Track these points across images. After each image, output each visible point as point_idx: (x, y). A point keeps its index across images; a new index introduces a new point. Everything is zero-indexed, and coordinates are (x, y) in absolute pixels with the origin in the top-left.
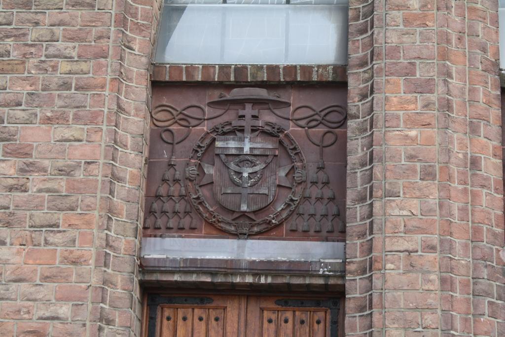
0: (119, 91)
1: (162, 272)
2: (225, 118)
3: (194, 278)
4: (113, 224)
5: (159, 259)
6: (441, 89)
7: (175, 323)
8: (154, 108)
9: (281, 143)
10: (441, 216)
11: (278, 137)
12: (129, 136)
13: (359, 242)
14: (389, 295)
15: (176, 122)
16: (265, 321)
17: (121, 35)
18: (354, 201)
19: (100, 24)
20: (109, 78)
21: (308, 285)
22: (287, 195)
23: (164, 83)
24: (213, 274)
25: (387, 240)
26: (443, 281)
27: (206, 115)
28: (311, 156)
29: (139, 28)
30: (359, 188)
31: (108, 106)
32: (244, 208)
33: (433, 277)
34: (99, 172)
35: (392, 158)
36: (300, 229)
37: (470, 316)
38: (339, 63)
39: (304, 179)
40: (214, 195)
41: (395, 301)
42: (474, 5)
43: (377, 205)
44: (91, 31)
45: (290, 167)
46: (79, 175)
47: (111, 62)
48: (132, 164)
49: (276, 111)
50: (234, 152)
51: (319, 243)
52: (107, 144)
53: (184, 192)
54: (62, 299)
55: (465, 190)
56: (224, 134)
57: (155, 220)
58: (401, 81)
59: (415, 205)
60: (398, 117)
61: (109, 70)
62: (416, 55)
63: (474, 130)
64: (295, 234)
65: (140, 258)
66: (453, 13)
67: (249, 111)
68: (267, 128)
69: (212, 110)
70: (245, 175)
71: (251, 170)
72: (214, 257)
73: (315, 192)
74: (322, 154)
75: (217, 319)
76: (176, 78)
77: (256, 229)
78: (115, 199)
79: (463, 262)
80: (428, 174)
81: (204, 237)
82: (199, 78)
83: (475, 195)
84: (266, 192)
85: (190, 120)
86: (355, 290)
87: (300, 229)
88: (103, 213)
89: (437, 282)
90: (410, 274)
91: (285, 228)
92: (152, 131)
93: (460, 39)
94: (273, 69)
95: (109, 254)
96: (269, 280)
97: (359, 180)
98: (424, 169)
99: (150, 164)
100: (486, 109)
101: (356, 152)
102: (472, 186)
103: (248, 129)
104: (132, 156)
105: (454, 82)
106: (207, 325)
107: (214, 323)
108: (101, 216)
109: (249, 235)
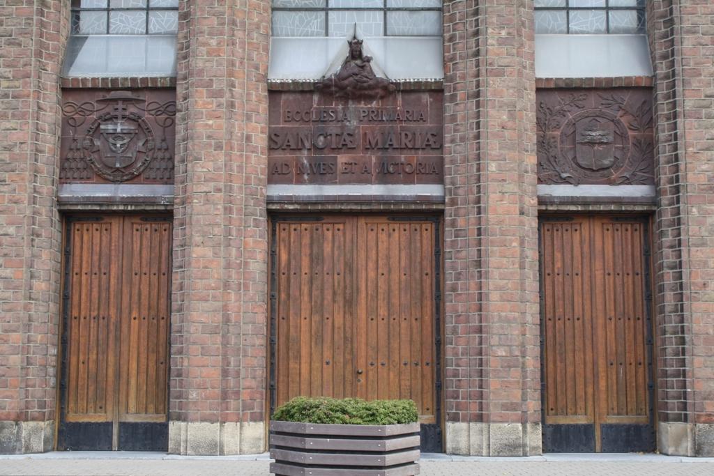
0: (38, 98)
1: (71, 205)
2: (107, 110)
3: (89, 208)
4: (39, 179)
5: (68, 197)
6: (228, 95)
7: (82, 232)
8: (63, 104)
9: (139, 125)
10: (226, 171)
11: (138, 121)
12: (46, 125)
13: (181, 186)
14: (194, 218)
15: (77, 113)
16: (134, 230)
17: (38, 63)
18: (178, 162)
19: (25, 56)
20: (32, 90)
21: (156, 210)
22: (143, 157)
23: (68, 90)
24: (100, 205)
25: (194, 186)
26: (225, 209)
27: (95, 109)
28: (157, 133)
29: (50, 57)
30: (182, 154)
31: (32, 108)
32: (118, 165)
33: (219, 207)
34: (28, 149)
35: (198, 137)
36: (151, 177)
37: (242, 228)
38: (173, 76)
39: (153, 147)
40: (100, 158)
41: (198, 221)
42: (251, 41)
43: (189, 165)
44: (20, 61)
45: (144, 140)
46: (17, 150)
47: (33, 80)
48: (49, 142)
49: (137, 106)
50: (111, 131)
51: (162, 185)
52: (37, 129)
53: (82, 157)
54: (10, 224)
55: (241, 155)
56: (106, 120)
57: (68, 170)
58: (204, 90)
59: (210, 165)
60: (202, 113)
61: (32, 85)
62: (213, 74)
63: (249, 118)
64: (149, 180)
65: (57, 196)
66: (238, 47)
67: (120, 105)
68: (132, 116)
69: (98, 105)
70: (118, 145)
71: (121, 143)
72: (101, 195)
73: (160, 154)
74: (164, 132)
75: (106, 230)
76: (76, 86)
77: (125, 178)
78: (39, 164)
79: (238, 197)
80: (219, 147)
81: (95, 183)
82: (90, 86)
83: (247, 157)
84: (131, 156)
85: (86, 112)
86: (178, 216)
87: (151, 177)
88: (31, 173)
89: (222, 210)
90: (206, 206)
91: (142, 177)
92: (63, 119)
93: (241, 63)
94: (134, 80)
95: (36, 197)
96: (133, 208)
97: (181, 149)
98: (216, 143)
99: (63, 140)
100: (257, 105)
101: (180, 132)
102: (246, 152)
103: (120, 117)
104: (49, 136)
105: (237, 90)
106: (101, 233)
107: (105, 232)
108: (30, 175)
109: (121, 182)
